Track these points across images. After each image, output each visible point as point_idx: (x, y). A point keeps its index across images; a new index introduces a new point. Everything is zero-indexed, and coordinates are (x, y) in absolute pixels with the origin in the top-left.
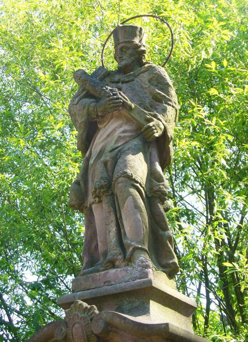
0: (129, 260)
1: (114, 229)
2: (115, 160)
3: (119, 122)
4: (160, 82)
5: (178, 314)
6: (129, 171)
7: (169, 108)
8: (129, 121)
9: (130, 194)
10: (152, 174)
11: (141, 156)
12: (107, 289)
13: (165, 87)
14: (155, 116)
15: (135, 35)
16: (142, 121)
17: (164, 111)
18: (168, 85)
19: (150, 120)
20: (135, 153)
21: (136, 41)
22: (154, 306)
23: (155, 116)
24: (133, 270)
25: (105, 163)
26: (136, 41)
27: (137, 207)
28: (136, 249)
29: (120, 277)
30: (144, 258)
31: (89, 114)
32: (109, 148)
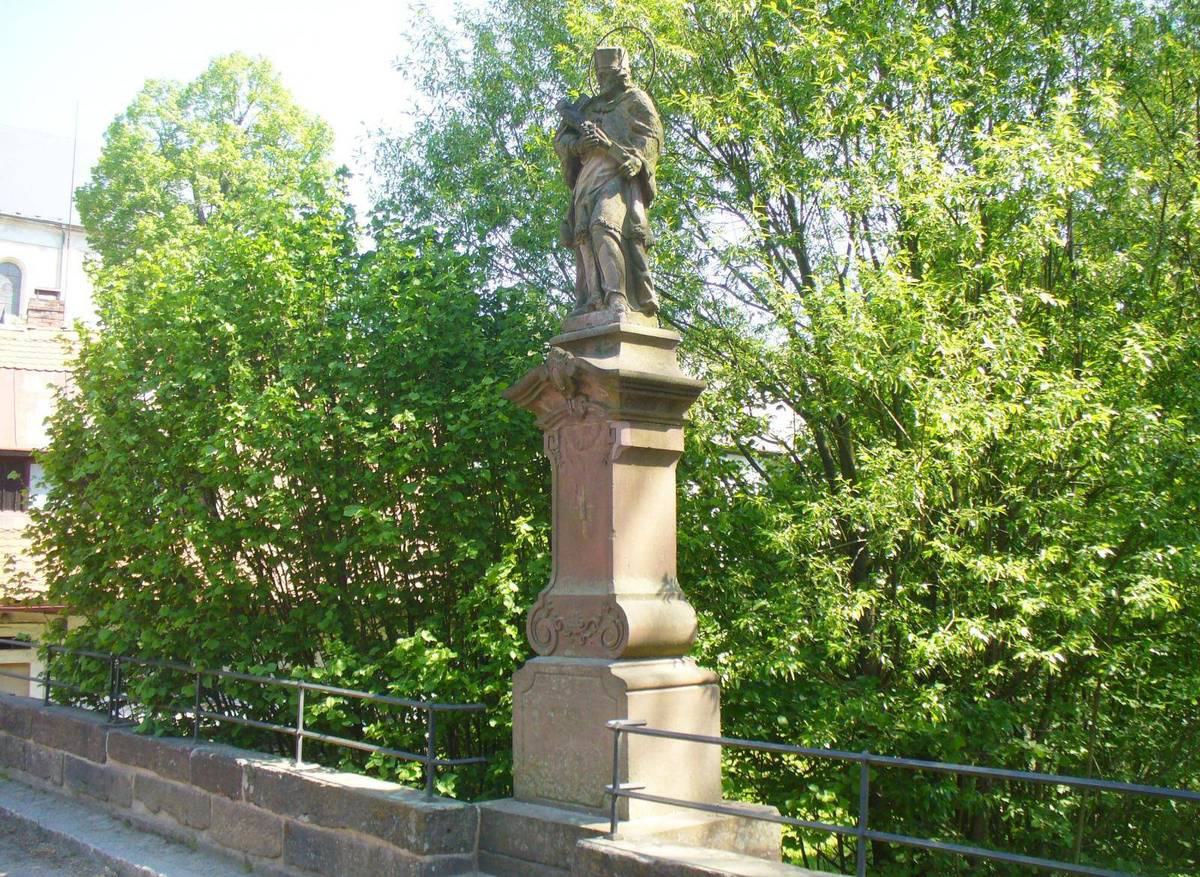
0: (607, 304)
1: (594, 273)
2: (595, 201)
3: (598, 161)
4: (641, 112)
5: (630, 764)
6: (602, 219)
7: (649, 140)
8: (608, 158)
9: (604, 242)
10: (631, 216)
11: (618, 197)
12: (589, 332)
13: (644, 115)
14: (633, 152)
15: (613, 59)
16: (619, 159)
17: (643, 144)
18: (649, 114)
19: (627, 158)
20: (611, 195)
21: (615, 65)
22: (625, 347)
23: (633, 152)
24: (609, 314)
25: (585, 207)
26: (615, 65)
27: (611, 254)
28: (612, 293)
29: (597, 320)
30: (623, 303)
31: (569, 152)
32: (588, 190)
